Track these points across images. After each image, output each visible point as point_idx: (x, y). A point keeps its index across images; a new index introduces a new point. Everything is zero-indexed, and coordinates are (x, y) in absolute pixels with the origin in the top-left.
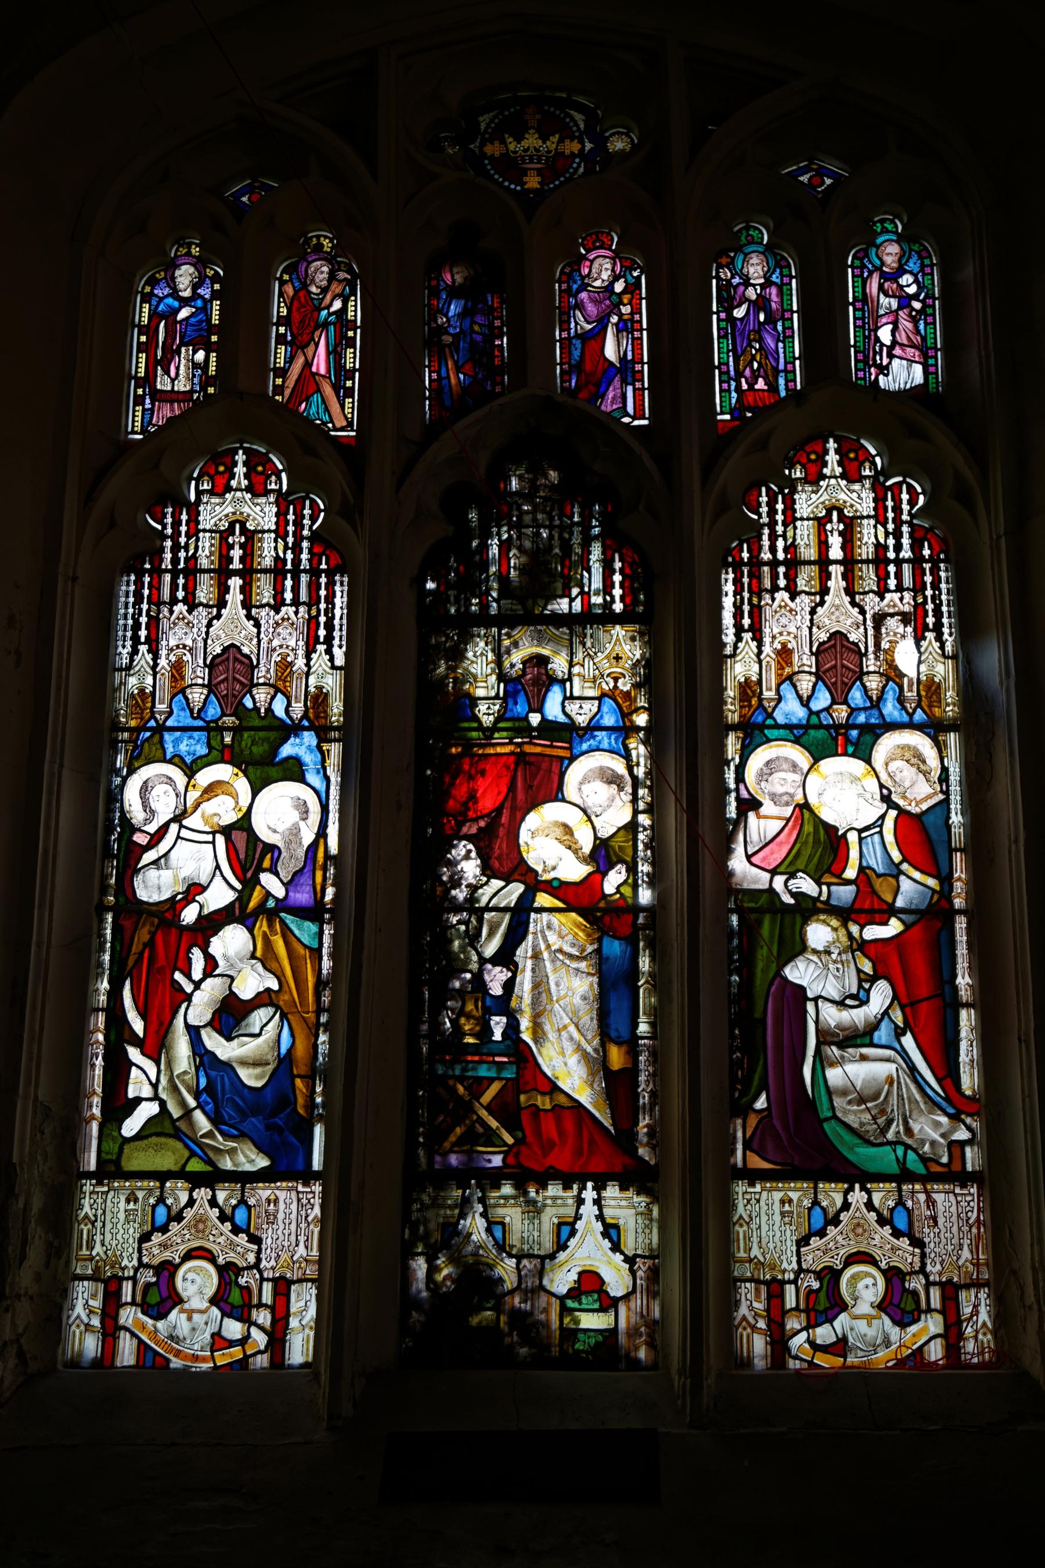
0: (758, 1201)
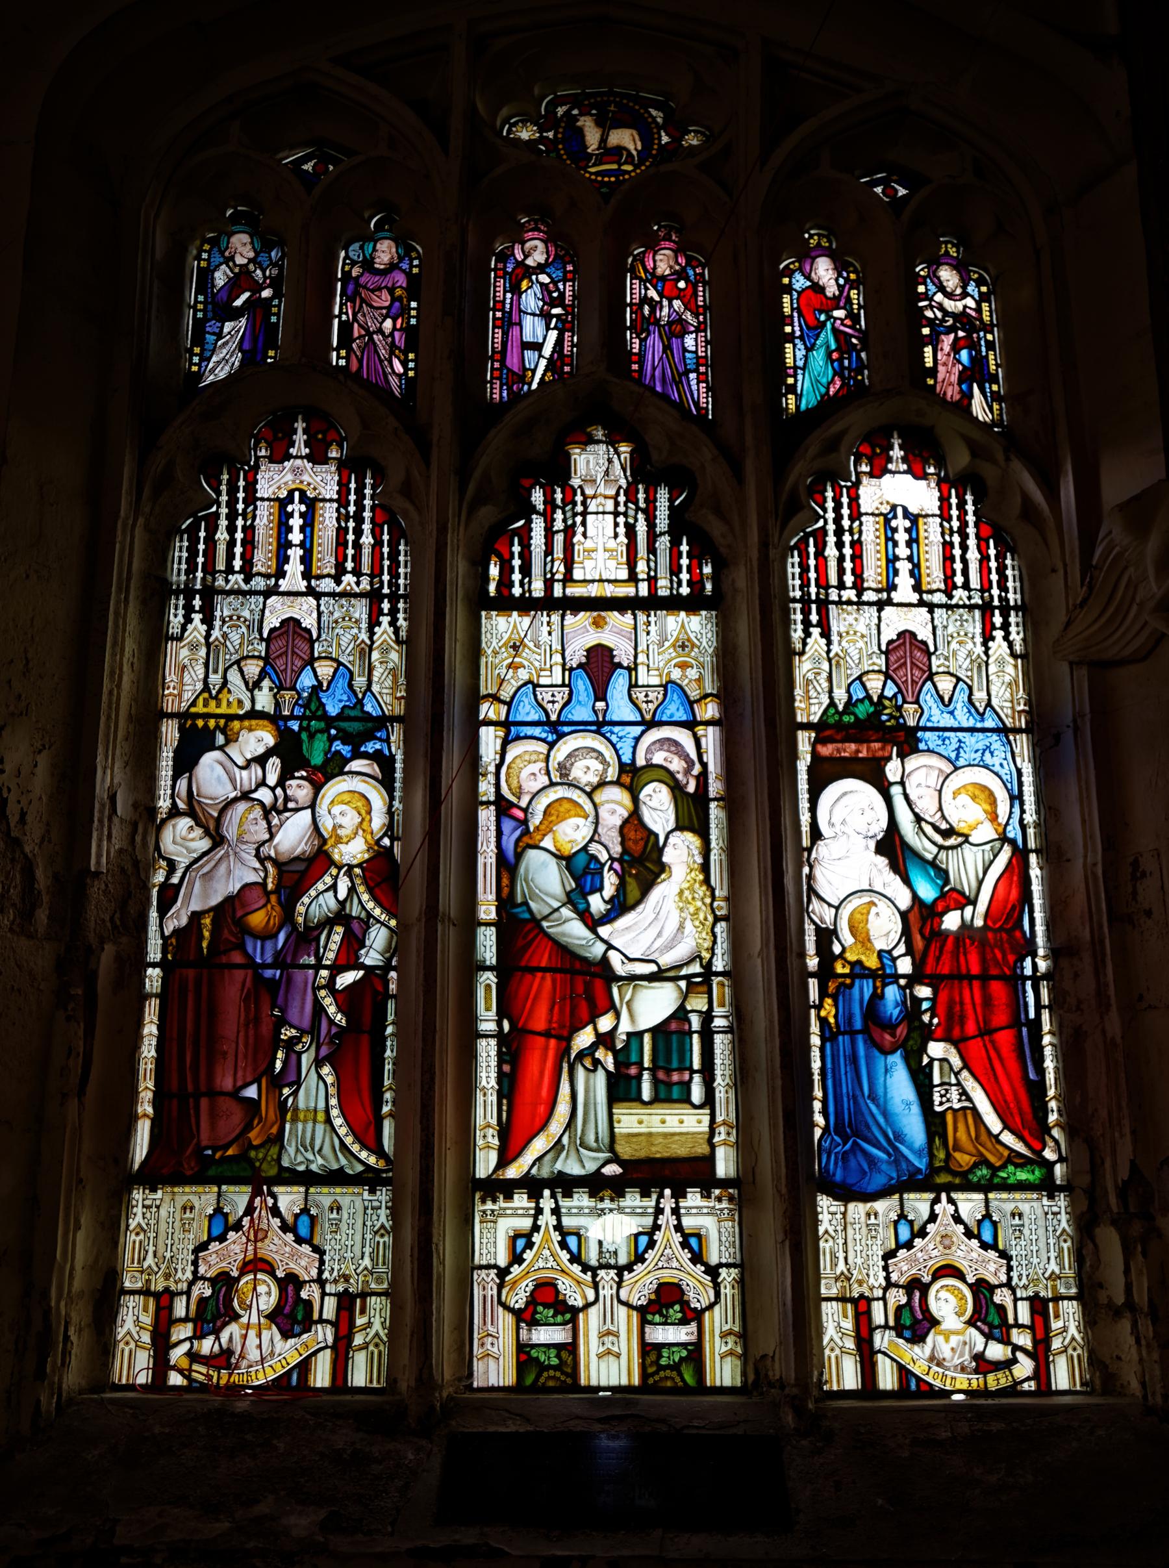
0: (158, 1207)
